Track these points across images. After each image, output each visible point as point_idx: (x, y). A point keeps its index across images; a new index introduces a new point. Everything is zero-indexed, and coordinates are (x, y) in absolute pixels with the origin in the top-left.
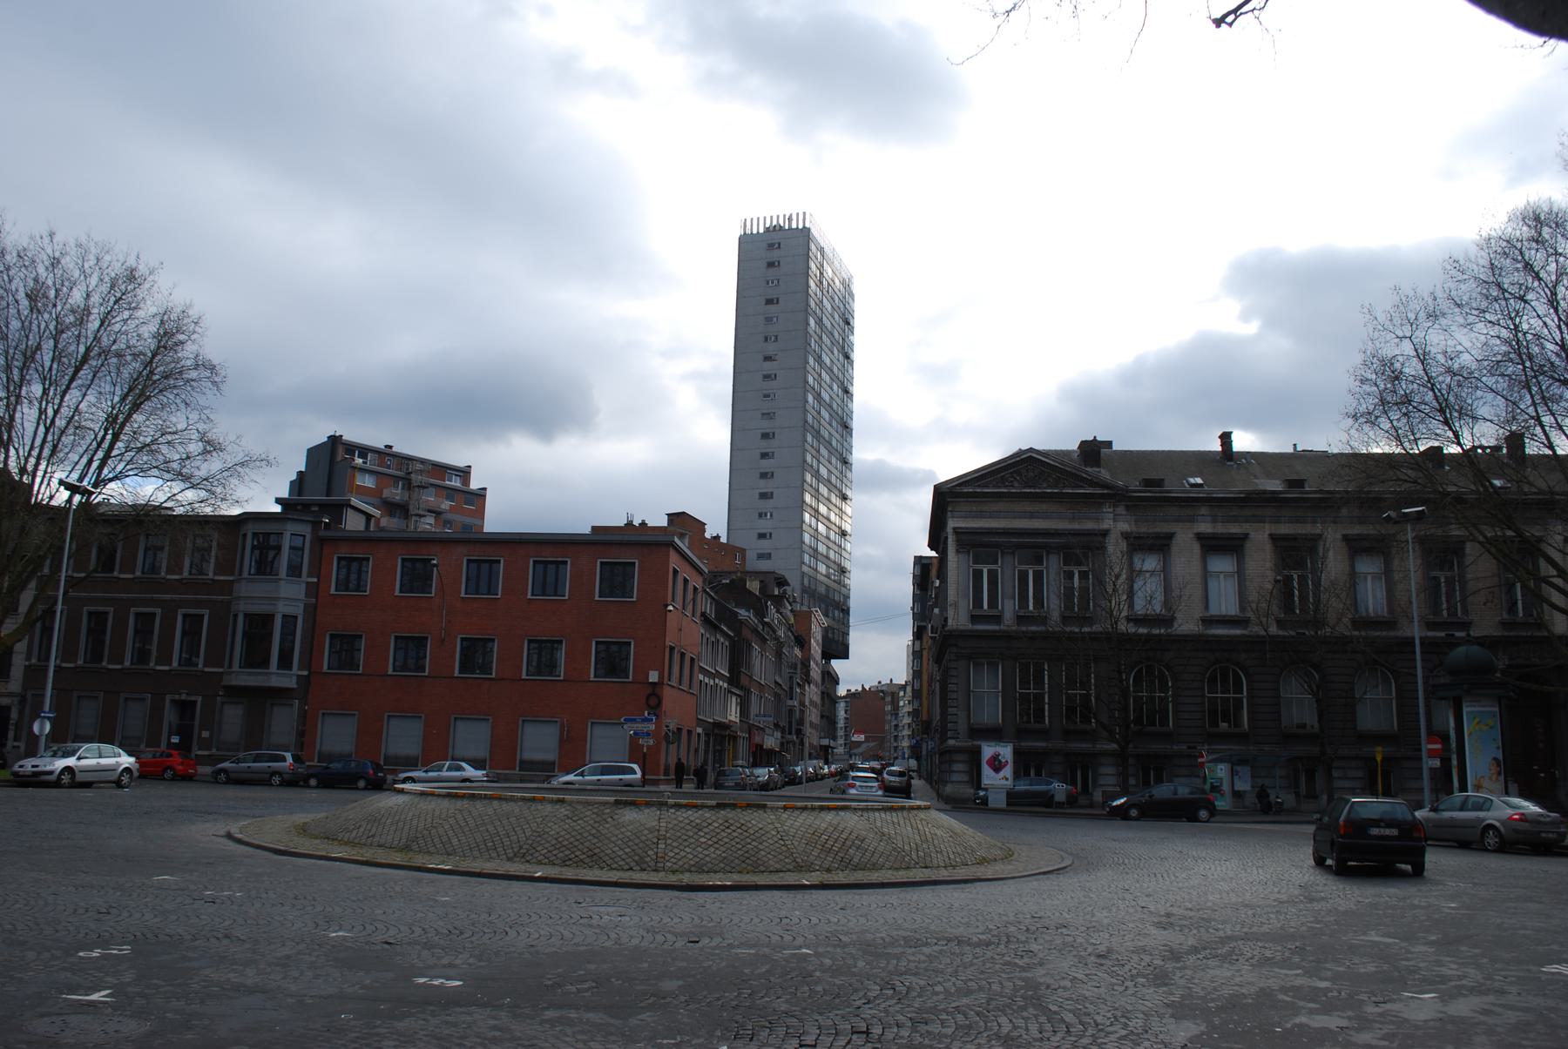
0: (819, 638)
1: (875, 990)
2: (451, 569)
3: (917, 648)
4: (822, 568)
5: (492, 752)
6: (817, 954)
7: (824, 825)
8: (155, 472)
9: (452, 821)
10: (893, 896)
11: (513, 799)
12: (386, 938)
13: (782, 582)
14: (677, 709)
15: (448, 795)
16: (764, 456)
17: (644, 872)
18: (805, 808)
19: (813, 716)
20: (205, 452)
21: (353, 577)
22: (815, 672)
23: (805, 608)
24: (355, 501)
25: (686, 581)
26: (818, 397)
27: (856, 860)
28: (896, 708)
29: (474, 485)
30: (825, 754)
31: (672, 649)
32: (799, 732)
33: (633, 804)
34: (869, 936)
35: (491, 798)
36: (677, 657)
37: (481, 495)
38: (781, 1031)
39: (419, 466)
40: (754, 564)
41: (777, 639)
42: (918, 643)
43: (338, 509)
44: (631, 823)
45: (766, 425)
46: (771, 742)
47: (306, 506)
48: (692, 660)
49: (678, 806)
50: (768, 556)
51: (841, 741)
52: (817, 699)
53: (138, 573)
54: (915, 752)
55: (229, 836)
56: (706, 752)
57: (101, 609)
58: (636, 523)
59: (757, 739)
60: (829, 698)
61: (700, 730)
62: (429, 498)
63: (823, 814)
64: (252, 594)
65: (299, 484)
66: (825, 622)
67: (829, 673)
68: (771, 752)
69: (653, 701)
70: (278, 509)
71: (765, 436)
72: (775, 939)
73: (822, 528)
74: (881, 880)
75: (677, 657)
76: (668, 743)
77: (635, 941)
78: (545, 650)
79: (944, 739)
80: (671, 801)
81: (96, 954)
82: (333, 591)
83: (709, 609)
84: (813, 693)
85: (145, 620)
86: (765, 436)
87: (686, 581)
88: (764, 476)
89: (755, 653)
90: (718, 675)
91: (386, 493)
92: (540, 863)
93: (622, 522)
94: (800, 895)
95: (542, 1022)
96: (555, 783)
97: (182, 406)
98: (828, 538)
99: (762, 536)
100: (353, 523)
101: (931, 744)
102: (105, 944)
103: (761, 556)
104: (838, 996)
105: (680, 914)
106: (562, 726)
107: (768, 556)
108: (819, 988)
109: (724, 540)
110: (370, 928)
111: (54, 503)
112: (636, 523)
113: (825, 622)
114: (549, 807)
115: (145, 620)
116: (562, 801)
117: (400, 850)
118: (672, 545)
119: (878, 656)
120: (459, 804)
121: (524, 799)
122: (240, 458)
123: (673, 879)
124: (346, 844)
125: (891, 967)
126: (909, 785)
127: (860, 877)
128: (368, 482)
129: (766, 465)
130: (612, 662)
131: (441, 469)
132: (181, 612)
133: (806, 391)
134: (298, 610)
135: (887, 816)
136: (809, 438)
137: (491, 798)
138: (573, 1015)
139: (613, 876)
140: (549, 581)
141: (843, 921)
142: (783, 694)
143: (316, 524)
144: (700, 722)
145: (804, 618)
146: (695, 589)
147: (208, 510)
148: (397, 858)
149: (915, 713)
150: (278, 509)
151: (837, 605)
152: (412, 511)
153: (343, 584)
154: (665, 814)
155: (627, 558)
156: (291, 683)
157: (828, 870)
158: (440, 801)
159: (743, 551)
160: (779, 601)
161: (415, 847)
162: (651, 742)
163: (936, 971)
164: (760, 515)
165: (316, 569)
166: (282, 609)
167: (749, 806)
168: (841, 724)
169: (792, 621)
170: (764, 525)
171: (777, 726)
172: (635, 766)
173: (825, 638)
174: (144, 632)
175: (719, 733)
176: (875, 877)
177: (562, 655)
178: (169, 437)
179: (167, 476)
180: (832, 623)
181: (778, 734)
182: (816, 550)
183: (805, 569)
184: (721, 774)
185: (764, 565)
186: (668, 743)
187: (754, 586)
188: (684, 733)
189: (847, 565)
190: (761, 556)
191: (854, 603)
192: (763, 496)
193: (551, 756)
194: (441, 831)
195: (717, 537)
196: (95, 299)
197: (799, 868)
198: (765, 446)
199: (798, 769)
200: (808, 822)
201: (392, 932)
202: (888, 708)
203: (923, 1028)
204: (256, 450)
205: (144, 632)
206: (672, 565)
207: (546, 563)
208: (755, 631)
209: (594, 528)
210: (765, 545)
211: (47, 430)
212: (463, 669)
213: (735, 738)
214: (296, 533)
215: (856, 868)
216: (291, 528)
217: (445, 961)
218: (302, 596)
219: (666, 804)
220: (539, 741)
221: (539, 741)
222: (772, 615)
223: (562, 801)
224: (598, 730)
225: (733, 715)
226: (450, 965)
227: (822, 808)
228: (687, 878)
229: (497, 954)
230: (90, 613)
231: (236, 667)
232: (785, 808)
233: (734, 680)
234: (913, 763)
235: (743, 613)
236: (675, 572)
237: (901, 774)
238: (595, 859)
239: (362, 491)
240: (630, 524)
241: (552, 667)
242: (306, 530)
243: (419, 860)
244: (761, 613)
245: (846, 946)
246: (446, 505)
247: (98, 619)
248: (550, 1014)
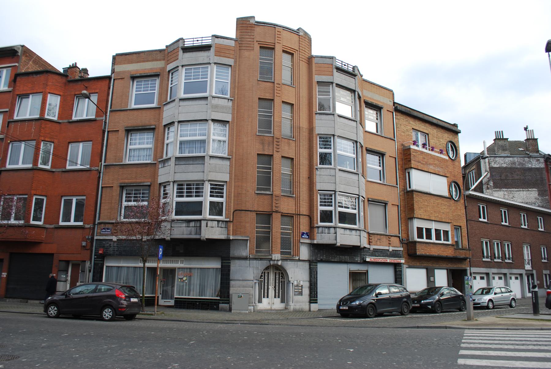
70: (62, 71)
132: (34, 198)
150: (62, 71)
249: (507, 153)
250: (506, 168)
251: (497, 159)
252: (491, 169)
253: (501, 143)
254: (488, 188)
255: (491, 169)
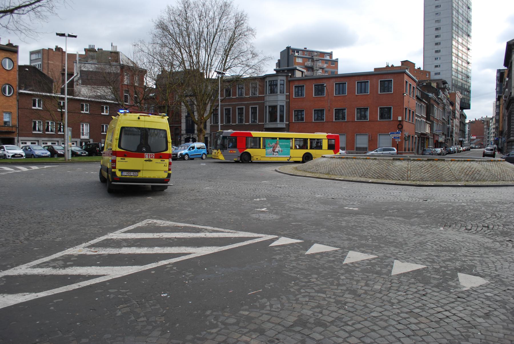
0: (459, 102)
1: (489, 216)
2: (330, 87)
3: (498, 104)
4: (460, 77)
5: (346, 145)
6: (468, 205)
7: (466, 166)
8: (240, 65)
9: (341, 165)
10: (492, 189)
11: (359, 159)
12: (332, 197)
13: (445, 83)
14: (408, 129)
15: (339, 158)
16: (437, 37)
17: (403, 181)
18: (459, 161)
19: (456, 130)
20: (253, 57)
21: (300, 92)
22: (457, 115)
23: (453, 92)
24: (298, 68)
25: (410, 85)
26: (458, 12)
27: (477, 178)
28: (488, 127)
29: (334, 58)
30: (461, 143)
31: (406, 109)
32: (451, 136)
33: (399, 159)
34: (485, 201)
35: (353, 158)
36: (408, 111)
37: (336, 62)
38: (460, 225)
39: (316, 54)
40: (433, 77)
41: (443, 103)
42: (498, 102)
43: (293, 71)
44: (398, 165)
45: (437, 25)
46: (441, 139)
47: (283, 71)
48: (413, 112)
49: (414, 160)
50: (439, 74)
51: (467, 139)
52: (458, 124)
53: (237, 96)
54: (496, 142)
55: (276, 171)
56: (418, 143)
57: (228, 107)
58: (390, 66)
59: (436, 139)
60: (463, 124)
61: (416, 136)
62: (320, 64)
63: (465, 163)
64: (270, 100)
65: (279, 64)
66: (461, 96)
67: (463, 115)
68: (441, 143)
69: (400, 127)
70: (275, 72)
71: (437, 29)
72: (452, 200)
73: (460, 62)
74: (486, 184)
75: (408, 111)
76: (406, 140)
77: (407, 200)
78: (362, 111)
79: (509, 137)
80: (412, 159)
81: (258, 200)
82: (294, 97)
83: (419, 94)
84: (456, 122)
85: (241, 109)
86: (437, 29)
87: (410, 85)
88: (437, 44)
89: (435, 109)
90: (422, 117)
91: (306, 64)
92: (370, 178)
93: (385, 66)
94: (458, 188)
95: (385, 219)
96: (368, 154)
97: (245, 43)
98: (462, 65)
99: (436, 66)
100: (298, 75)
101: (503, 139)
102: (259, 197)
103: (436, 74)
104: (476, 217)
105: (421, 192)
106: (369, 136)
107: (439, 74)
108: (470, 214)
109: (422, 69)
110: (326, 195)
111: (213, 78)
112: (390, 66)
113: (461, 96)
114: (371, 161)
115: (241, 109)
116: (376, 159)
117: (327, 174)
118: (405, 73)
119: (483, 107)
120: (343, 160)
121: (363, 159)
122: (263, 58)
123: (414, 183)
124: (310, 172)
125: (494, 210)
126: (494, 154)
127: (479, 183)
128: (300, 60)
129: (438, 40)
130: (385, 113)
131: (323, 54)
132: (250, 107)
133: (452, 10)
134: (284, 104)
135: (489, 163)
136: (454, 28)
137: (353, 158)
138: (393, 218)
139: (394, 182)
140: (362, 89)
141: (475, 196)
142: (446, 123)
143: (287, 76)
144: (416, 133)
145: (454, 95)
146: (414, 87)
147: (256, 75)
148: (326, 176)
149: (496, 128)
150: (275, 72)
151: (466, 91)
152: (315, 69)
153: (297, 94)
154: (410, 163)
155: (388, 78)
156: (284, 126)
157: (467, 181)
158: (337, 159)
159: (429, 73)
160: (443, 89)
161: (331, 173)
162: (400, 140)
163: (510, 211)
164: (436, 59)
165: (289, 91)
166: (279, 104)
167: (439, 160)
168: (467, 133)
169: (449, 97)
170: (437, 62)
171: (443, 134)
172: (395, 148)
173: (461, 102)
174: (241, 114)
175: (423, 137)
176: (484, 183)
177: (368, 113)
178: (242, 54)
179: (243, 66)
180: (465, 97)
181: (444, 137)
182: (457, 70)
183: (453, 77)
184: (424, 150)
185: (437, 77)
186: (406, 140)
187: (434, 85)
188: (411, 138)
189: (470, 75)
190: (436, 74)
191: (472, 89)
192: (437, 52)
193: (366, 146)
194: (338, 168)
195: (420, 68)
196: (216, 14)
197: (457, 180)
198: (437, 33)
199: (451, 149)
200: (460, 165)
201: (333, 196)
202: (485, 127)
203: (507, 227)
204: (268, 55)
205: (241, 114)
206: (405, 80)
207: (361, 82)
208: (435, 101)
209: (375, 69)
210: (438, 70)
211: (209, 56)
212: (336, 119)
213: (428, 138)
214: (281, 80)
215: (477, 180)
216: (280, 78)
217: (351, 203)
218: (285, 99)
219: (410, 159)
220: (362, 141)
221: (362, 141)
222: (441, 95)
223: (376, 159)
224: (381, 137)
225: (428, 130)
226: (353, 204)
227: (465, 161)
228: (418, 183)
229: (365, 202)
230: (226, 109)
231: (267, 122)
232: (451, 161)
233: (428, 118)
234: (495, 146)
235: (431, 95)
236: (406, 82)
237: (491, 150)
238: (387, 177)
239: (299, 64)
240: (388, 66)
241: (365, 117)
242: (284, 78)
243: (333, 177)
244: (437, 94)
245: (477, 203)
246: (325, 66)
247: (228, 110)
248: (386, 217)
249: (95, 61)
250: (92, 72)
251: (87, 65)
252: (82, 72)
253: (91, 53)
254: (77, 85)
255: (82, 72)
